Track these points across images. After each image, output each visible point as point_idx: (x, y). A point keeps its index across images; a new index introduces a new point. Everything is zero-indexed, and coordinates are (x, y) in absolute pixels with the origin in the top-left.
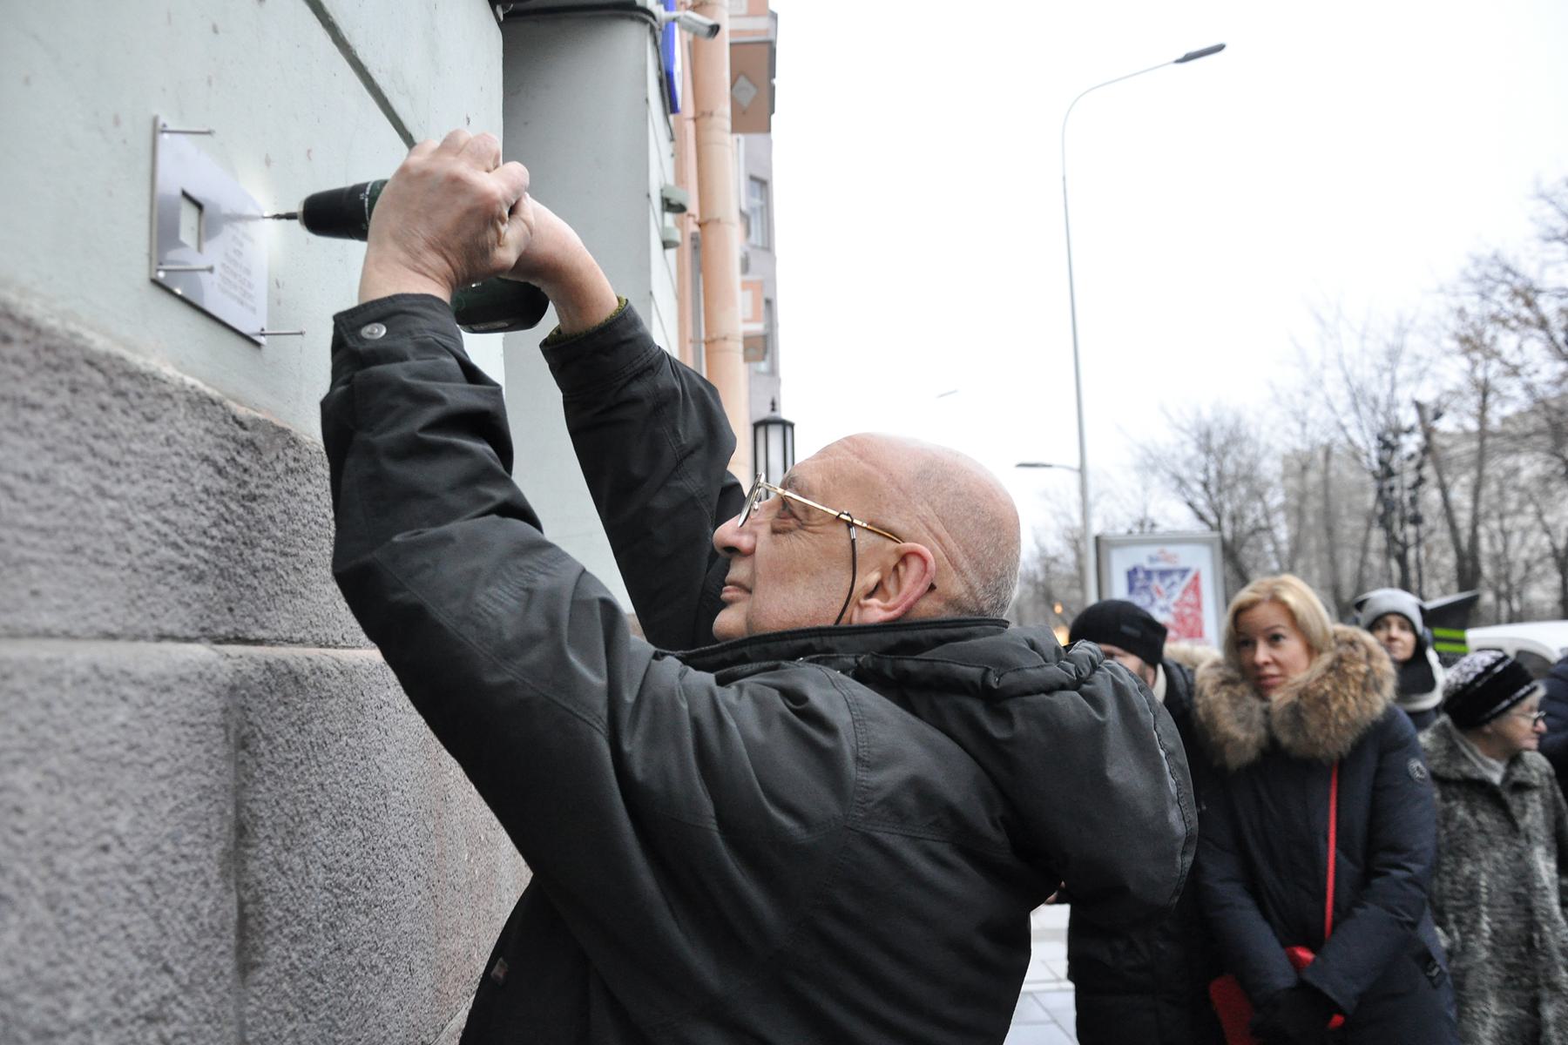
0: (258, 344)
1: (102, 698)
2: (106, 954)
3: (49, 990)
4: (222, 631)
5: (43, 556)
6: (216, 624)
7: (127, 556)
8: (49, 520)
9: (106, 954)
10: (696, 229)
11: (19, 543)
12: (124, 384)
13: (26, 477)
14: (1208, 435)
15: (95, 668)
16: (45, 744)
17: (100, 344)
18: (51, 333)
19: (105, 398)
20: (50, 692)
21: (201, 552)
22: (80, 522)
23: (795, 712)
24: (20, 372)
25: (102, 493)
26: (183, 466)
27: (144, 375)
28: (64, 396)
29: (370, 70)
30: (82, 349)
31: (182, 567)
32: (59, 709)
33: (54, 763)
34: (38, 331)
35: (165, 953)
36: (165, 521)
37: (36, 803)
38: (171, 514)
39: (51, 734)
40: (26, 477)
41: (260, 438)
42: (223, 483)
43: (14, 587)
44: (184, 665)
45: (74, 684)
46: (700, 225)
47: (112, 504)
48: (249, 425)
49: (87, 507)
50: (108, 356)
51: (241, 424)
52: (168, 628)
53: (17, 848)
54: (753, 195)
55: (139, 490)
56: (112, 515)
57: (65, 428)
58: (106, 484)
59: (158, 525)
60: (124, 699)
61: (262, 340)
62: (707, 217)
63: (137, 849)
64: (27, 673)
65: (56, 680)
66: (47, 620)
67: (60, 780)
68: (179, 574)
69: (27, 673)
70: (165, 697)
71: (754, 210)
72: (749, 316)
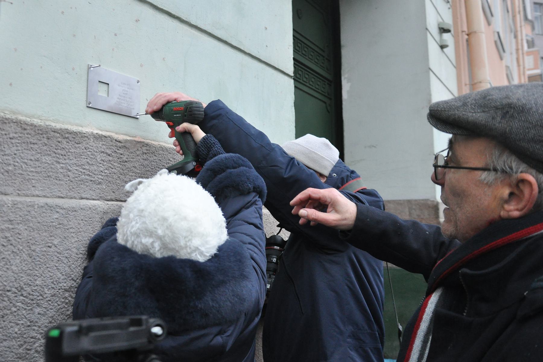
0: (137, 118)
1: (49, 211)
2: (49, 271)
3: (29, 275)
4: (109, 198)
5: (37, 178)
6: (106, 196)
7: (69, 178)
8: (39, 170)
9: (49, 271)
10: (466, 37)
11: (29, 175)
12: (67, 135)
13: (31, 160)
14: (213, 118)
15: (47, 204)
16: (28, 220)
17: (58, 126)
18: (40, 126)
19: (60, 140)
20: (29, 209)
21: (100, 177)
22: (50, 170)
23: (519, 243)
24: (30, 136)
25: (59, 163)
26: (92, 155)
27: (76, 133)
28: (45, 140)
29: (199, 26)
30: (51, 129)
31: (91, 181)
32: (33, 213)
33: (31, 225)
34: (36, 126)
35: (73, 276)
36: (84, 169)
37: (25, 234)
38: (87, 167)
39: (30, 218)
40: (31, 160)
41: (128, 145)
42: (111, 158)
43: (27, 185)
44: (84, 205)
45: (38, 207)
46: (468, 35)
47: (62, 165)
48: (123, 142)
49: (53, 166)
50: (61, 129)
51: (120, 142)
52: (84, 196)
53: (19, 242)
54: (536, 11)
55: (74, 161)
56: (62, 168)
57: (45, 148)
58: (60, 161)
59: (81, 170)
60: (57, 212)
61: (138, 117)
62: (470, 31)
63: (61, 249)
64: (23, 204)
65: (33, 206)
66: (37, 193)
67: (33, 229)
68: (91, 182)
69: (23, 204)
70: (74, 213)
71: (536, 18)
72: (532, 66)
